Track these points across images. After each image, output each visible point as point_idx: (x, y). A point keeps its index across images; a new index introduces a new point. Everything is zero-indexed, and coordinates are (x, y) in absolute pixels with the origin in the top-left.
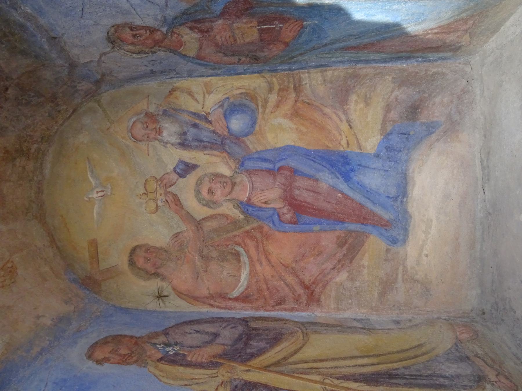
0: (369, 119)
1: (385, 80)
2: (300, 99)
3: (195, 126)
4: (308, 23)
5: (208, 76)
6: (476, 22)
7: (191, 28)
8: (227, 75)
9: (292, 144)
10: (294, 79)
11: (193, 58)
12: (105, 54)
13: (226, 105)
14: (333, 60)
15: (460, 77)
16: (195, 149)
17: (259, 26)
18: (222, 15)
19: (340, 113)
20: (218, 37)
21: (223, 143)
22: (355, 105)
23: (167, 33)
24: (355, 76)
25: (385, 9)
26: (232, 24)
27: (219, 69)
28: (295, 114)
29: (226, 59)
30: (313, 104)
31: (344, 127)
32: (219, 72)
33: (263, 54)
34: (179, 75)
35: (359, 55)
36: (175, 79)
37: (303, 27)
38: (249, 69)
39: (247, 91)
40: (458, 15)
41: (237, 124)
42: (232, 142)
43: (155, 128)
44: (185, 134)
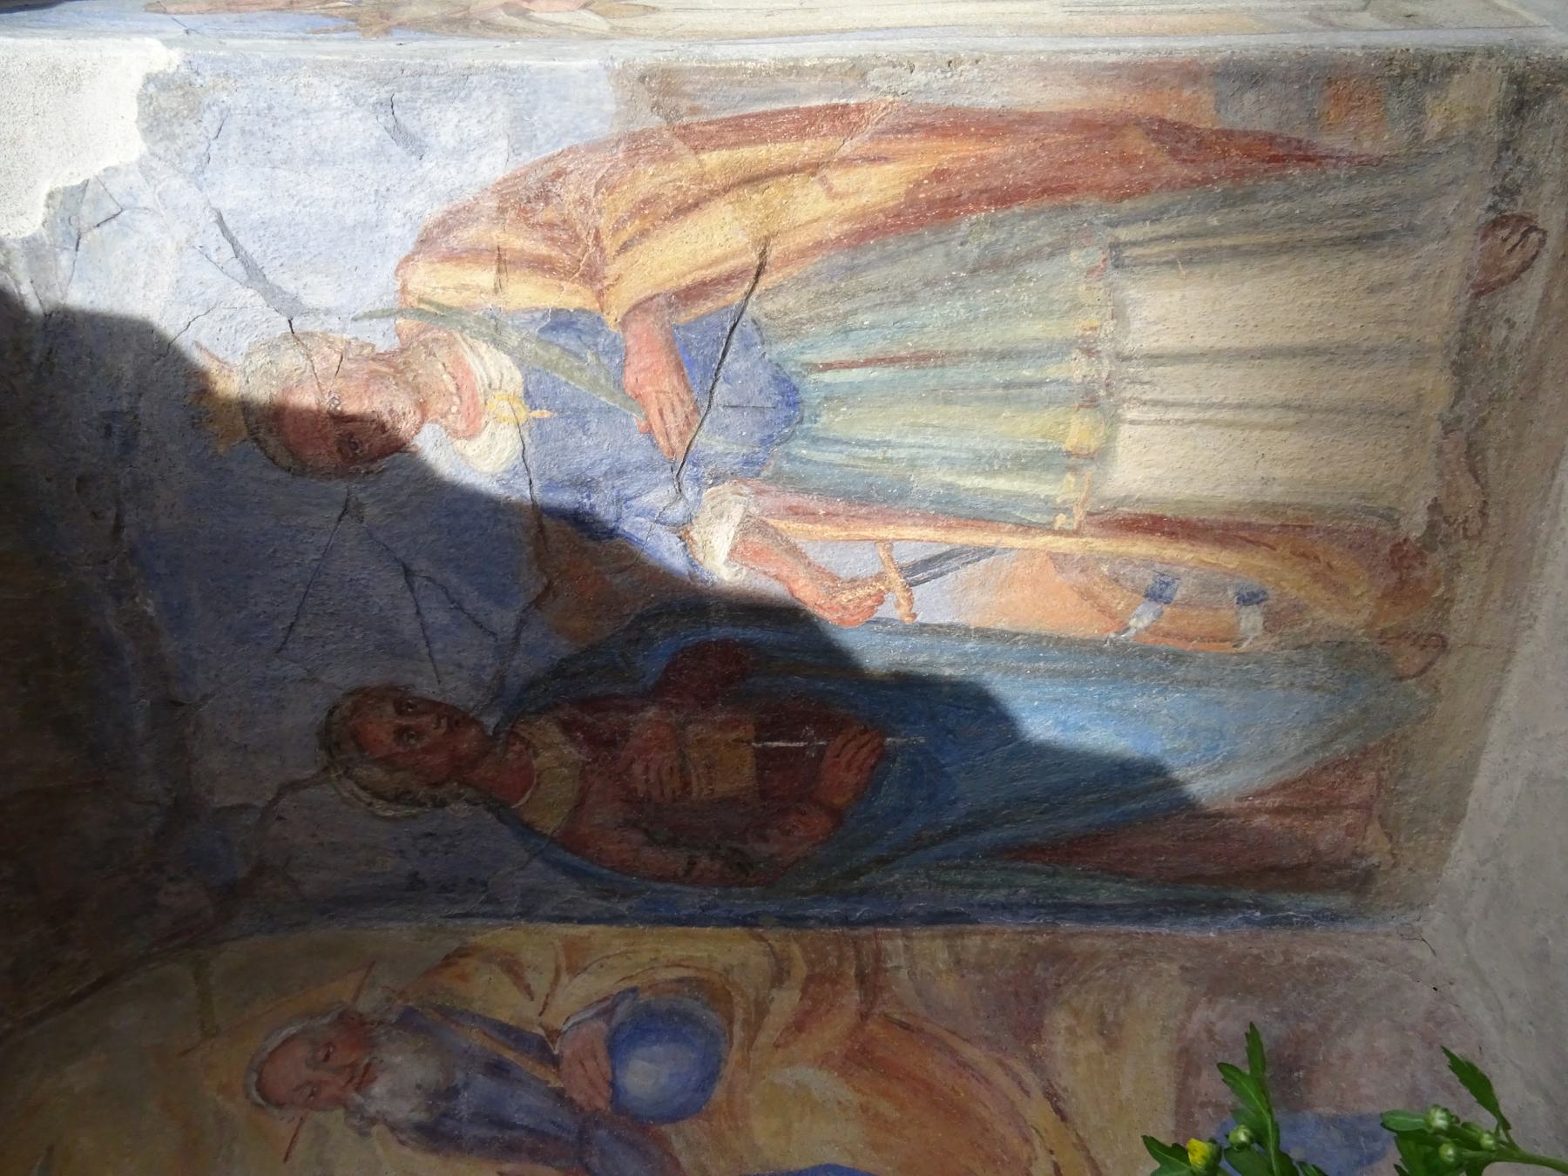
0: (1126, 1091)
1: (1158, 974)
2: (876, 1011)
3: (497, 1069)
4: (899, 741)
5: (583, 921)
6: (1385, 774)
7: (567, 727)
8: (644, 922)
9: (845, 1161)
10: (858, 952)
11: (552, 840)
12: (295, 786)
13: (622, 1011)
14: (981, 896)
15: (1407, 978)
16: (471, 1151)
17: (758, 739)
18: (656, 693)
19: (1019, 1067)
20: (638, 768)
21: (583, 1139)
22: (1068, 1044)
23: (496, 732)
24: (1057, 956)
25: (1110, 708)
26: (683, 727)
27: (624, 896)
28: (859, 1059)
29: (648, 853)
30: (921, 1030)
31: (1038, 1112)
32: (622, 908)
33: (764, 849)
34: (495, 909)
35: (1060, 881)
36: (477, 922)
37: (884, 755)
38: (716, 906)
39: (704, 976)
40: (1325, 745)
41: (648, 1074)
42: (619, 1138)
43: (353, 1066)
44: (452, 1092)
